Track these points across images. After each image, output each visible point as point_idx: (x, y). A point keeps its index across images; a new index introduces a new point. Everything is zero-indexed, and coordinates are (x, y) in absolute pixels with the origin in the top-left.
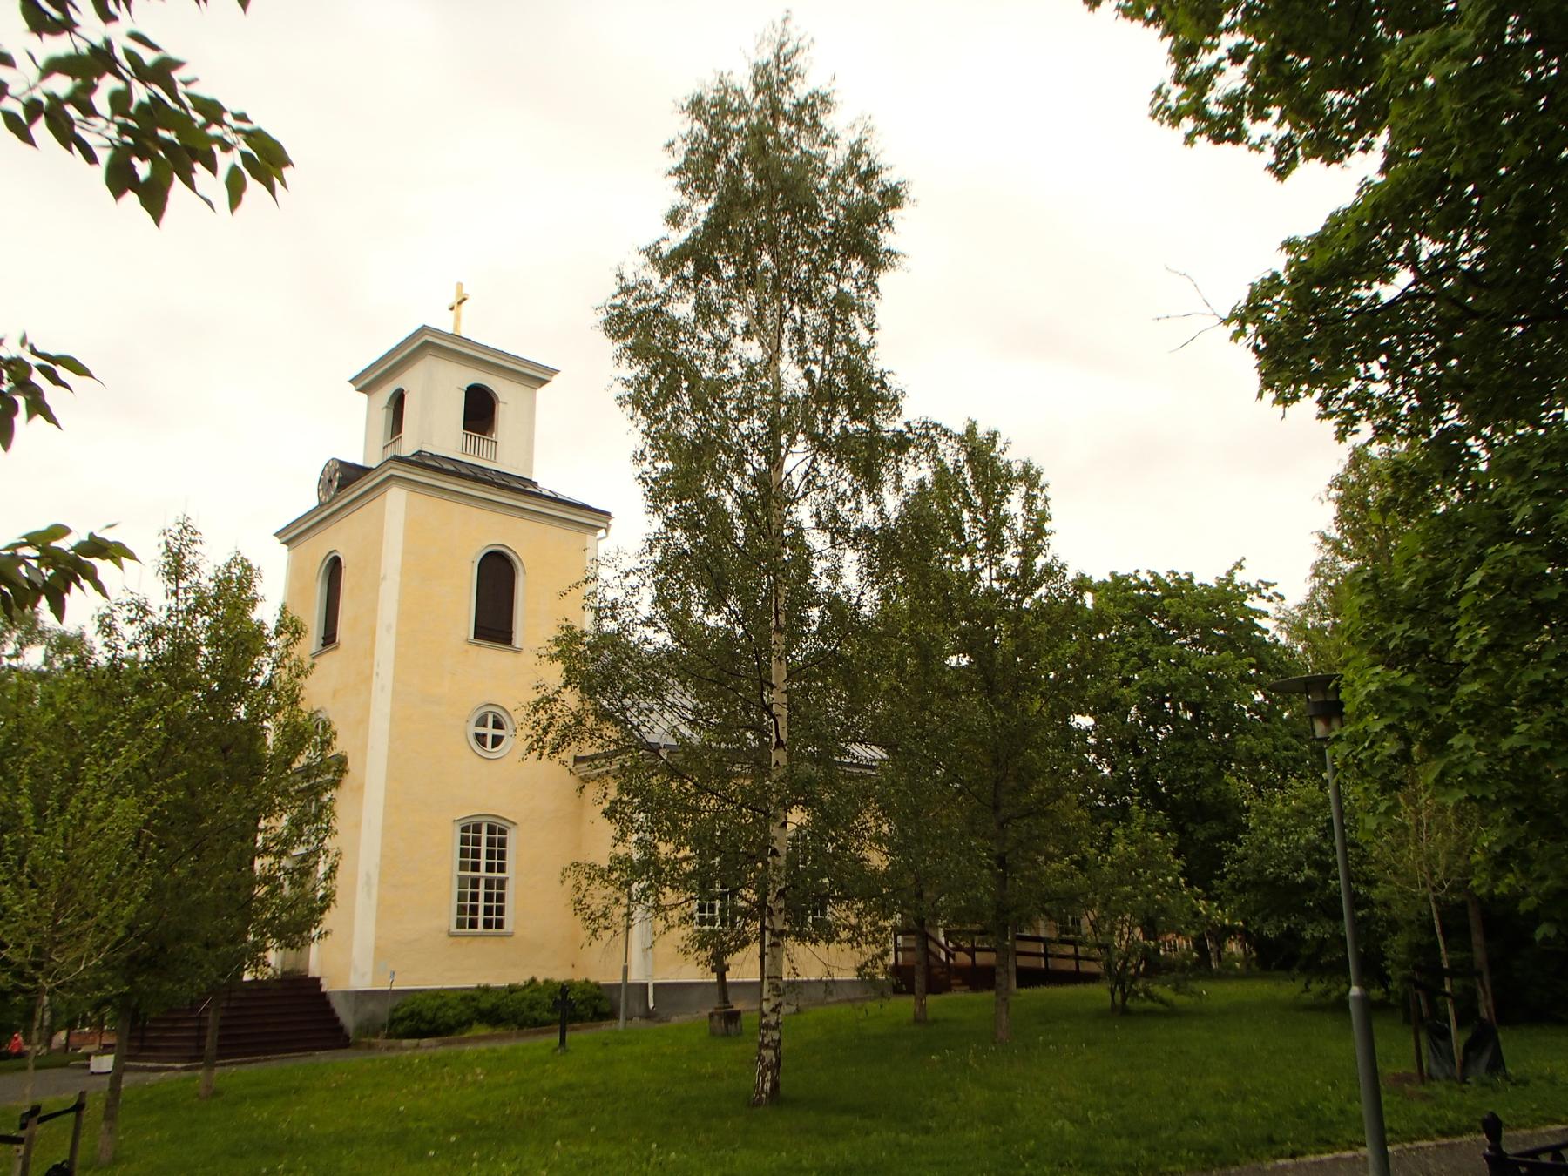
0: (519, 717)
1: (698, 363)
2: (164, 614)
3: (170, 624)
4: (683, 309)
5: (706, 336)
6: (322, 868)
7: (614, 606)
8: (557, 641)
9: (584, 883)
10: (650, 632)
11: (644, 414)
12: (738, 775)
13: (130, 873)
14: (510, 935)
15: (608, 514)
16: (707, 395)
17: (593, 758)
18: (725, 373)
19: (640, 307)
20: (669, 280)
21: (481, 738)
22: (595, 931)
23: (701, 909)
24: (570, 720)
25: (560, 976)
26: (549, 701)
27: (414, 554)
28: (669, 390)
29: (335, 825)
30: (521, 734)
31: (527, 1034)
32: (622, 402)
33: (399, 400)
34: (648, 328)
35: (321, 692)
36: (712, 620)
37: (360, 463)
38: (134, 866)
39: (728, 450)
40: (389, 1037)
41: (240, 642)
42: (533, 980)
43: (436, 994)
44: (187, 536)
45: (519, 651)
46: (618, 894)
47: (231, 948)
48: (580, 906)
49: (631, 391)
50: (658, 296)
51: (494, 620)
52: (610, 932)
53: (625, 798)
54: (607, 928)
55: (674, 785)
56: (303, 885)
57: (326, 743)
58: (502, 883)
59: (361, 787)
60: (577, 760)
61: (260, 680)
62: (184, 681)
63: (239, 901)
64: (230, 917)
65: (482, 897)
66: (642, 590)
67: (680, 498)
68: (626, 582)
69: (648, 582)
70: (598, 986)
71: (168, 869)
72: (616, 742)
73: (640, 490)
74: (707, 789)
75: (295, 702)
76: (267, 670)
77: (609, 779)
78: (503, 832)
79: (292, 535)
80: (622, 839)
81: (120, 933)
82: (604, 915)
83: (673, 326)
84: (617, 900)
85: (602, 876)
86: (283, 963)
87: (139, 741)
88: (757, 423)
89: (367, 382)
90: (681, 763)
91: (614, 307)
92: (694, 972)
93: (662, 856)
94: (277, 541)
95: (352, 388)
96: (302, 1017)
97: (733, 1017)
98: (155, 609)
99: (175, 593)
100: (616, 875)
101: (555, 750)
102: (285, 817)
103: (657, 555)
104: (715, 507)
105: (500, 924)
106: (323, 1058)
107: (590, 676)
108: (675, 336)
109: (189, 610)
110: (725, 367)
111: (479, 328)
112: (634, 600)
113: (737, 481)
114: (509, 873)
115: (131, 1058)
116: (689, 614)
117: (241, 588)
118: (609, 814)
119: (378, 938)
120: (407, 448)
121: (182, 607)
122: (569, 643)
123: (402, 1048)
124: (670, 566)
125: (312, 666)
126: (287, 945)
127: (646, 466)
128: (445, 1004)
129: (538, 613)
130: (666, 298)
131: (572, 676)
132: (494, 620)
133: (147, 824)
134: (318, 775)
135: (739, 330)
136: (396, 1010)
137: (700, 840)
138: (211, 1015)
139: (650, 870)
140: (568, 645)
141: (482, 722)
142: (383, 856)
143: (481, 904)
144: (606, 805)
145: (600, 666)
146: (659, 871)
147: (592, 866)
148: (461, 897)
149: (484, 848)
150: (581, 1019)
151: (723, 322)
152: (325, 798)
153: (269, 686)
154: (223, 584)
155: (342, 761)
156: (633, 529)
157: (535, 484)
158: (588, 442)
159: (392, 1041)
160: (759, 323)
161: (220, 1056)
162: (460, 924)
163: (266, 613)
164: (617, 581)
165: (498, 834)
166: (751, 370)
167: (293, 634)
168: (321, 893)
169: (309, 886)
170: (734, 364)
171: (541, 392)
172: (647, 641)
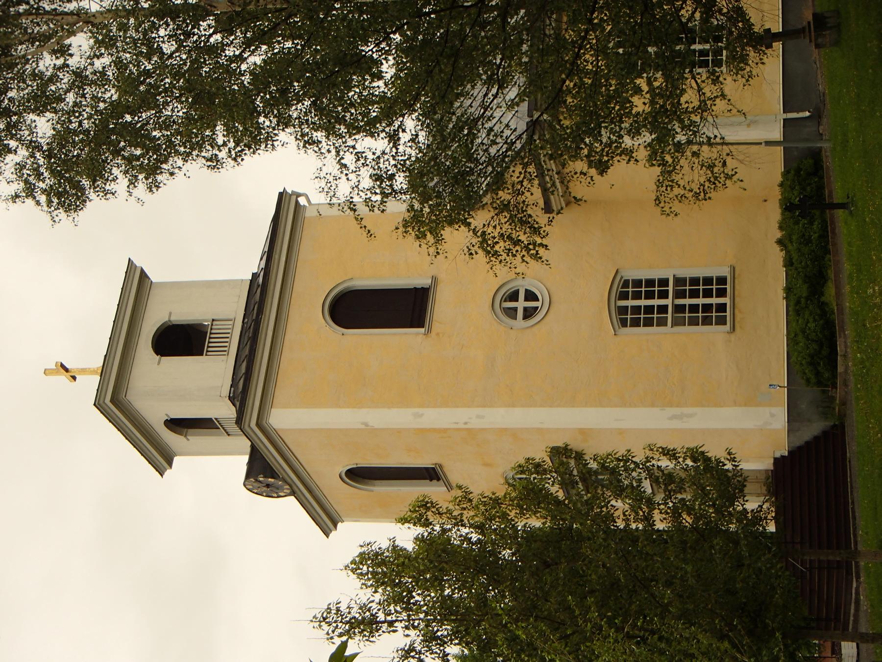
0: (503, 273)
1: (102, 105)
2: (412, 633)
3: (422, 625)
4: (43, 126)
5: (71, 98)
6: (665, 463)
7: (377, 178)
8: (421, 236)
9: (676, 191)
10: (405, 137)
11: (166, 161)
12: (558, 29)
13: (668, 642)
14: (733, 269)
15: (281, 195)
16: (138, 92)
17: (545, 192)
18: (110, 73)
19: (46, 174)
20: (13, 144)
21: (529, 313)
22: (728, 177)
23: (704, 64)
24: (504, 217)
25: (775, 213)
26: (484, 241)
27: (336, 396)
28: (138, 136)
29: (622, 452)
30: (522, 267)
31: (834, 244)
32: (154, 186)
33: (177, 425)
34: (69, 164)
35: (486, 478)
36: (388, 69)
37: (246, 458)
38: (661, 639)
39: (196, 65)
40: (834, 386)
41: (435, 558)
42: (780, 242)
43: (792, 340)
44: (333, 616)
45: (435, 279)
46: (689, 154)
47: (743, 542)
48: (701, 195)
49: (141, 177)
50: (32, 156)
51: (405, 308)
52: (729, 160)
53: (586, 152)
54: (724, 164)
55: (569, 100)
56: (682, 480)
57: (538, 467)
58: (679, 281)
59: (582, 432)
60: (548, 209)
61: (475, 537)
62: (478, 607)
63: (694, 541)
64: (712, 547)
65: (694, 301)
66: (359, 148)
67: (254, 113)
68: (352, 167)
69: (350, 143)
70: (785, 174)
71: (665, 609)
72: (525, 166)
73: (249, 160)
74: (573, 63)
75: (496, 502)
76: (464, 531)
77: (566, 170)
78: (626, 284)
79: (326, 519)
80: (629, 153)
81: (726, 644)
82: (711, 167)
83: (63, 137)
84: (695, 154)
85: (670, 173)
86: (758, 495)
87: (538, 643)
88: (162, 32)
89: (161, 458)
90: (545, 95)
91: (49, 203)
92: (771, 67)
93: (647, 109)
94: (333, 534)
95: (168, 473)
96: (810, 473)
97: (819, 21)
98: (408, 641)
99: (391, 624)
100: (668, 158)
101: (536, 230)
102: (613, 502)
103: (319, 135)
104: (261, 76)
105: (722, 280)
106: (853, 449)
107: (456, 199)
108: (75, 133)
109: (406, 609)
110: (103, 73)
111: (91, 348)
112: (370, 156)
113: (230, 52)
114: (668, 273)
115: (845, 628)
116: (383, 97)
117: (383, 563)
118: (603, 168)
119: (735, 404)
120: (226, 411)
121: (404, 615)
122: (422, 223)
123: (846, 371)
124: (333, 120)
125: (460, 487)
126: (742, 491)
127: (222, 154)
128: (803, 331)
129: (397, 264)
130: (33, 146)
131: (458, 216)
132: (405, 308)
133: (619, 629)
134: (571, 474)
135: (60, 62)
136: (808, 381)
137: (629, 69)
138: (807, 558)
139: (664, 118)
140: (423, 225)
141: (511, 313)
142: (653, 405)
143: (701, 301)
144: (593, 172)
145: (445, 189)
146: (663, 111)
147: (659, 184)
148: (694, 322)
149: (643, 302)
150: (820, 188)
151: (53, 79)
152: (594, 465)
153: (480, 528)
154: (379, 581)
155: (556, 452)
156: (289, 165)
157: (255, 276)
158: (206, 219)
159: (839, 381)
160: (49, 38)
161: (848, 546)
162: (722, 321)
163: (407, 537)
164: (352, 176)
165: (628, 288)
166: (105, 42)
167: (428, 509)
168: (689, 462)
169: (683, 475)
170: (98, 64)
171: (155, 276)
172: (414, 139)
